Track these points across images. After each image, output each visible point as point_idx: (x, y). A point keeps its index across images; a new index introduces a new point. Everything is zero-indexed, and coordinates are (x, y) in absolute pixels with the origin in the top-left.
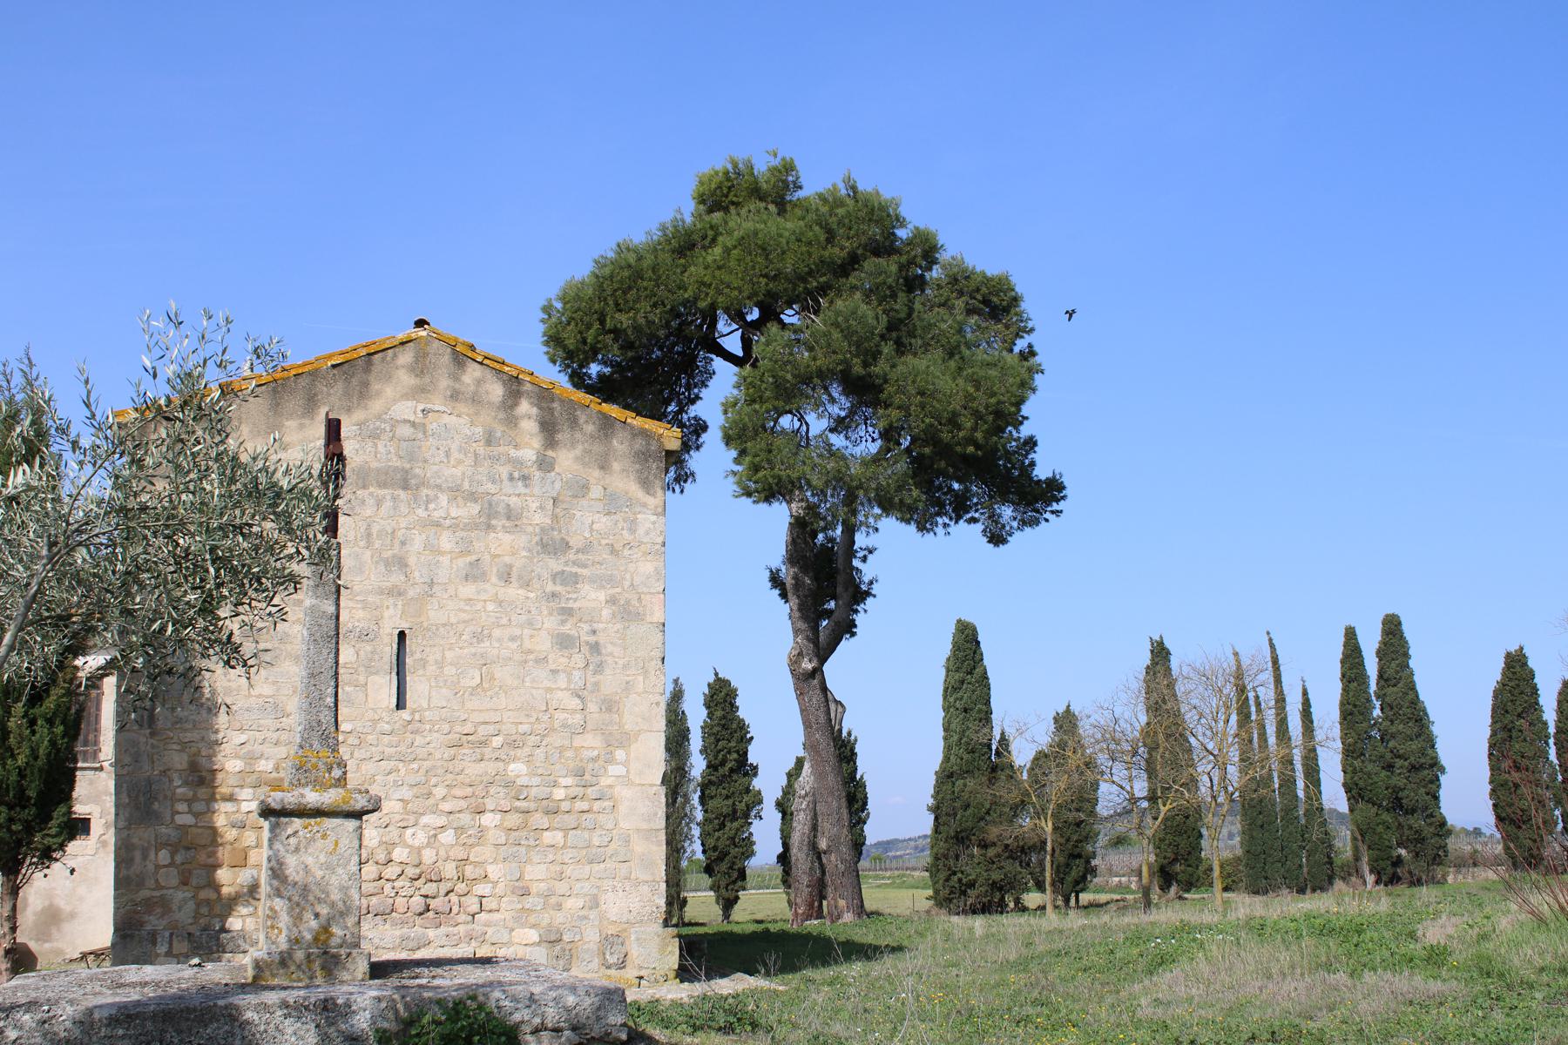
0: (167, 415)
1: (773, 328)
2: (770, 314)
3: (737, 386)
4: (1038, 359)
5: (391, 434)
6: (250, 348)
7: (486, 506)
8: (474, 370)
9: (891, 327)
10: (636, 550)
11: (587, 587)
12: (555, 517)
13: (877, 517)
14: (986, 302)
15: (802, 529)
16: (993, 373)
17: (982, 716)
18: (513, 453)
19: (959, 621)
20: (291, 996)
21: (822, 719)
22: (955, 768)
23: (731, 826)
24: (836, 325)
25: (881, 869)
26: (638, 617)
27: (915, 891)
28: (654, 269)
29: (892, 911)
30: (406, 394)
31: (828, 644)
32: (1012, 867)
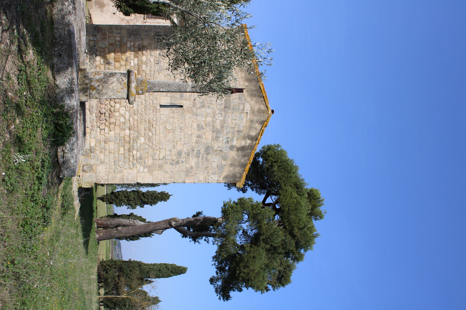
0: (242, 50)
1: (274, 213)
2: (278, 211)
3: (257, 202)
4: (266, 292)
5: (240, 103)
6: (263, 72)
7: (220, 131)
8: (259, 127)
9: (275, 248)
10: (207, 175)
11: (196, 160)
12: (216, 151)
13: (217, 244)
14: (282, 276)
15: (214, 221)
16: (261, 278)
17: (158, 276)
18: (235, 138)
19: (187, 268)
20: (75, 81)
21: (157, 228)
22: (142, 267)
23: (125, 200)
24: (275, 232)
25: (112, 244)
26: (187, 175)
27: (105, 255)
28: (291, 177)
29: (99, 248)
30: (252, 108)
31: (180, 229)
32: (112, 285)
